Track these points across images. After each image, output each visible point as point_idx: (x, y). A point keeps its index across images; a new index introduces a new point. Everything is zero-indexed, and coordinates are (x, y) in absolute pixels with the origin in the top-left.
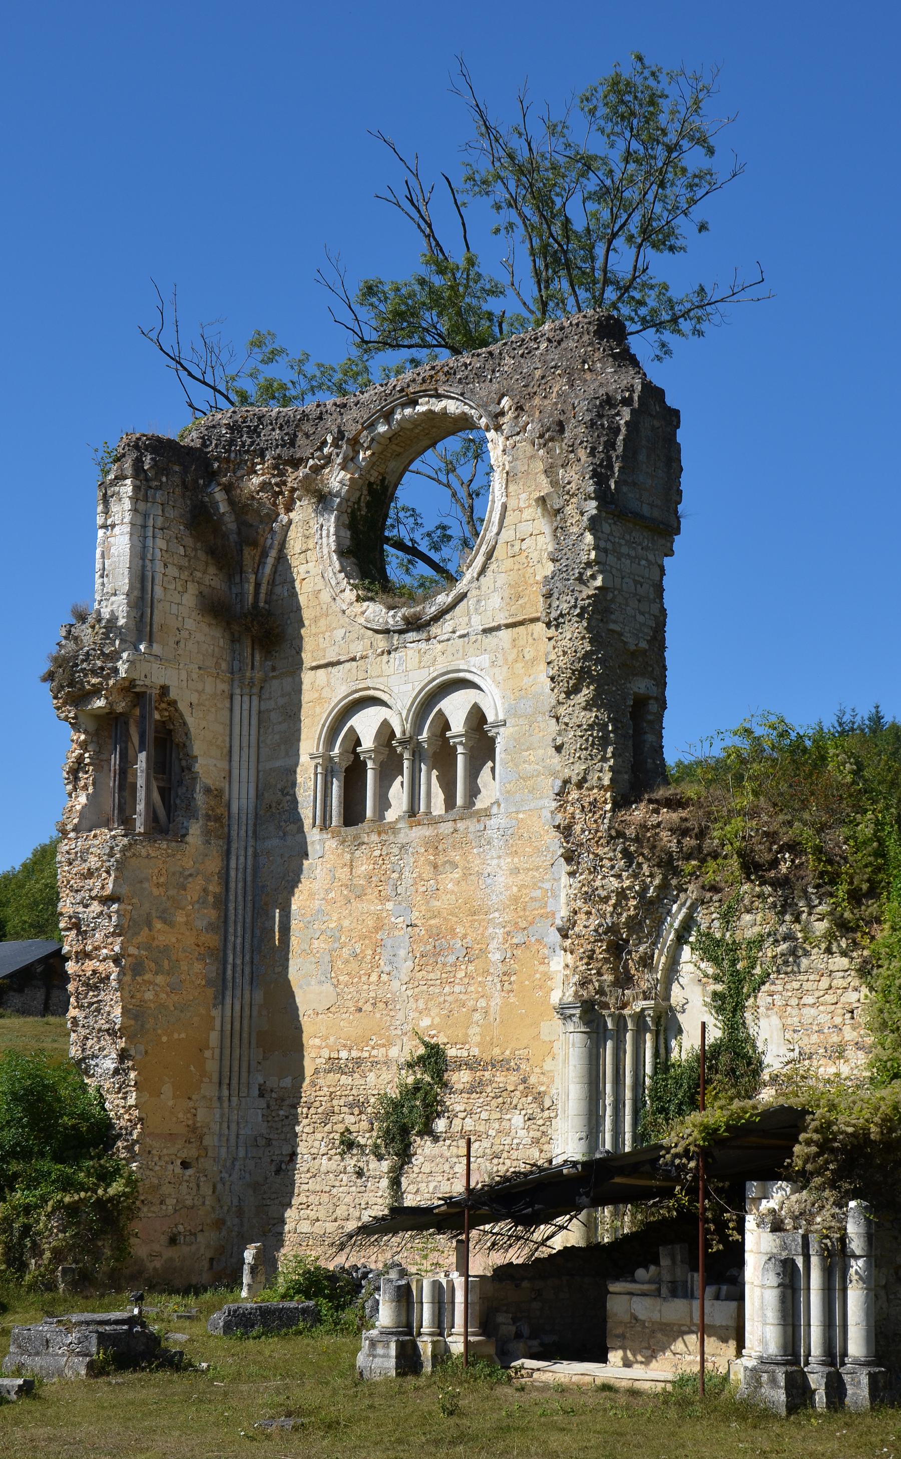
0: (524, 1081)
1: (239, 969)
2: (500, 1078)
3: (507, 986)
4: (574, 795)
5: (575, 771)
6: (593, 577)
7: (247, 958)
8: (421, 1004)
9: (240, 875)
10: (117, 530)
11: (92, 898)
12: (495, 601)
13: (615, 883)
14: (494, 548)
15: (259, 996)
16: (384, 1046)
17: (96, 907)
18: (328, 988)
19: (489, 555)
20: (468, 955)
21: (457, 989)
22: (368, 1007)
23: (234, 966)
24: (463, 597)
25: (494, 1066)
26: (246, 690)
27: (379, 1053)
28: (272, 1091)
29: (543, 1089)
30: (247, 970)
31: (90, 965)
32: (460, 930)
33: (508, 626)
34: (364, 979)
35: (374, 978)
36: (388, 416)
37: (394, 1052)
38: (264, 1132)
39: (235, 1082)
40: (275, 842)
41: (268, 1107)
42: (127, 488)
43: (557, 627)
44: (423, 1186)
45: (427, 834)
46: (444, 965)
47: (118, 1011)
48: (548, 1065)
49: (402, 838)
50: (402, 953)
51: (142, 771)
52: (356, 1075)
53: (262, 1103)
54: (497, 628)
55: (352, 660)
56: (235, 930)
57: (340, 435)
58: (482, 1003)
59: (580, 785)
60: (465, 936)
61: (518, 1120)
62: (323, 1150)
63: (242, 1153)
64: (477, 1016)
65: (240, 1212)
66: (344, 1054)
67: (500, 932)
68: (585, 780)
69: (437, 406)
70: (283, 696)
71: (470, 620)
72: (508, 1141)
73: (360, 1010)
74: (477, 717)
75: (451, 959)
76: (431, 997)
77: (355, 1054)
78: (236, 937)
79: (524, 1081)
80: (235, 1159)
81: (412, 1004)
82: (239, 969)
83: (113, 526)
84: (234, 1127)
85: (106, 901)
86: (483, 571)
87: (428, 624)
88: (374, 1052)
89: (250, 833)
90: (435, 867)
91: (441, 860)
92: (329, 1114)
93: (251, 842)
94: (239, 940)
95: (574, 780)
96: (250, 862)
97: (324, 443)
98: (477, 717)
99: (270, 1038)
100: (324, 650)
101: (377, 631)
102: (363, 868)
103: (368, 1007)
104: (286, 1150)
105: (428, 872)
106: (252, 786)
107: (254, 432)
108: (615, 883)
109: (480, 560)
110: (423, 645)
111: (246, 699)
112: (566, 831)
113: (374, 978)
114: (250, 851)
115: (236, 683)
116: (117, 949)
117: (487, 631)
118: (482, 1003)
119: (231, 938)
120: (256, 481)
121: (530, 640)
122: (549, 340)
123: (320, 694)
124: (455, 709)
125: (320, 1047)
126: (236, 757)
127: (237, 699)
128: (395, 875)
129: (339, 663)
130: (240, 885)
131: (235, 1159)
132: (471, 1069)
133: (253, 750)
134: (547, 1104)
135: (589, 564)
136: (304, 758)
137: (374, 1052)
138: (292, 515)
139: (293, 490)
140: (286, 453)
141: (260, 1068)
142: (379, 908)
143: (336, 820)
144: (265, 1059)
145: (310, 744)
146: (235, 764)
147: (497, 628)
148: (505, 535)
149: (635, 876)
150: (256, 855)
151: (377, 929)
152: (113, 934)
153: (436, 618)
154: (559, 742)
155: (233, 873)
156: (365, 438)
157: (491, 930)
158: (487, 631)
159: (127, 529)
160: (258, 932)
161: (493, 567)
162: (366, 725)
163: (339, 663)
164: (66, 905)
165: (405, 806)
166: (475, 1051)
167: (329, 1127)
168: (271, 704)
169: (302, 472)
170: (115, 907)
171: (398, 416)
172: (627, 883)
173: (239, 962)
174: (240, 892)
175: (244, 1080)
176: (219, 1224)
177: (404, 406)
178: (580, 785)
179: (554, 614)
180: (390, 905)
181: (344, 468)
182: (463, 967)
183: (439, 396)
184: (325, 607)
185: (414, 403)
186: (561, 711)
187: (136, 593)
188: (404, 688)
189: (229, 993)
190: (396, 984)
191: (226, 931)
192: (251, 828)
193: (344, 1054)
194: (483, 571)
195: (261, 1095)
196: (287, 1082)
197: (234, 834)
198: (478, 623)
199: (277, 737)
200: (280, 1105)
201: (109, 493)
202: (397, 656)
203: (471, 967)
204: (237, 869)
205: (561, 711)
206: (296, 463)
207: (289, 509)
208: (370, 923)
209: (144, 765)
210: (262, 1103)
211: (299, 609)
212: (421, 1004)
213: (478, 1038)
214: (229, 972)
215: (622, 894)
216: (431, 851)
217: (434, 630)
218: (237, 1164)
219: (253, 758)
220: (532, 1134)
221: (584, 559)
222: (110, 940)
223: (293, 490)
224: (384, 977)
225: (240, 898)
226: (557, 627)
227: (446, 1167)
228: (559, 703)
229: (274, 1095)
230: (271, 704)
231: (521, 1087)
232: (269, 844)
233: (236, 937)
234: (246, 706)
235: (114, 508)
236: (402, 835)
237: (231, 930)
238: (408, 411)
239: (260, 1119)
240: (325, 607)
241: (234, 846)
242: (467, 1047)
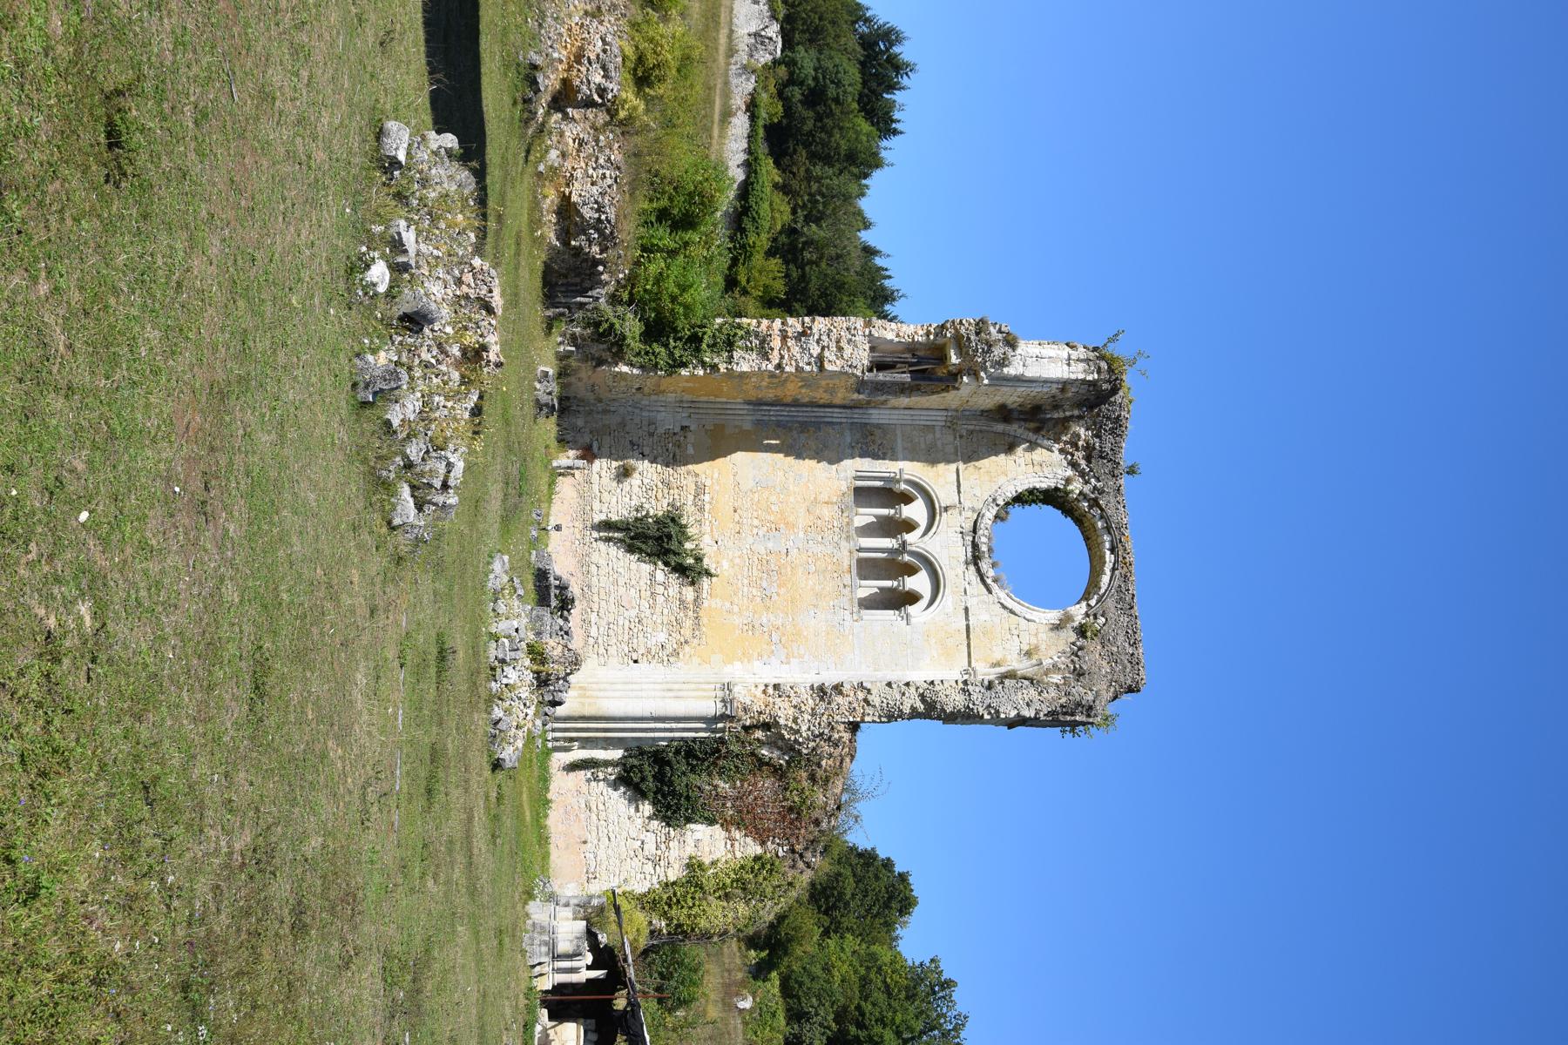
2: (688, 623)
4: (861, 695)
5: (875, 699)
8: (737, 561)
13: (804, 728)
17: (816, 350)
18: (751, 484)
19: (1012, 612)
22: (737, 518)
24: (990, 592)
31: (776, 343)
33: (968, 627)
35: (756, 522)
36: (1108, 529)
40: (848, 439)
48: (696, 660)
49: (844, 544)
53: (677, 430)
54: (967, 619)
57: (1101, 492)
58: (736, 609)
59: (866, 701)
64: (728, 604)
65: (605, 412)
66: (707, 498)
67: (779, 623)
69: (1108, 568)
75: (765, 585)
77: (707, 507)
81: (738, 553)
85: (820, 359)
87: (976, 564)
95: (870, 698)
97: (1098, 480)
99: (717, 444)
103: (737, 518)
104: (647, 451)
107: (1112, 432)
108: (804, 728)
112: (838, 688)
113: (756, 522)
117: (966, 609)
118: (736, 609)
120: (1082, 431)
123: (940, 478)
124: (919, 582)
135: (997, 712)
140: (1095, 453)
151: (787, 524)
153: (978, 570)
156: (1096, 512)
158: (966, 609)
159: (1066, 376)
161: (1005, 613)
162: (915, 511)
164: (821, 324)
166: (706, 604)
168: (938, 435)
171: (1106, 537)
180: (801, 535)
183: (1113, 570)
185: (1112, 550)
186: (913, 689)
190: (750, 540)
196: (691, 450)
200: (673, 451)
205: (913, 689)
206: (1088, 459)
207: (1061, 451)
208: (791, 519)
210: (677, 430)
215: (798, 732)
217: (972, 568)
230: (938, 435)
232: (847, 434)
235: (1081, 366)
238: (1107, 545)
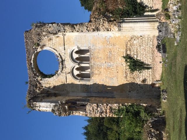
0: (129, 41)
2: (128, 45)
3: (115, 45)
5: (85, 28)
6: (59, 25)
10: (41, 105)
11: (97, 109)
12: (60, 48)
14: (53, 48)
15: (115, 92)
17: (99, 109)
20: (110, 52)
21: (115, 54)
29: (130, 38)
32: (107, 53)
33: (64, 46)
34: (113, 71)
35: (113, 69)
36: (32, 68)
43: (65, 30)
44: (145, 59)
46: (112, 56)
47: (115, 105)
49: (93, 65)
54: (64, 47)
57: (34, 77)
59: (88, 28)
60: (108, 52)
61: (135, 42)
62: (139, 79)
64: (119, 50)
66: (124, 75)
67: (107, 46)
68: (87, 27)
72: (138, 44)
73: (118, 72)
74: (77, 52)
76: (116, 59)
77: (124, 73)
79: (129, 41)
83: (40, 106)
85: (98, 107)
86: (56, 50)
87: (62, 60)
88: (124, 69)
92: (134, 78)
95: (87, 28)
97: (34, 80)
98: (77, 52)
100: (64, 80)
101: (62, 70)
105: (98, 60)
107: (31, 91)
113: (113, 69)
116: (105, 104)
117: (65, 50)
122: (27, 39)
123: (70, 80)
124: (75, 56)
125: (123, 80)
126: (78, 95)
127: (69, 95)
129: (66, 77)
132: (127, 51)
134: (133, 37)
136: (79, 83)
137: (124, 69)
138: (44, 86)
139: (40, 86)
143: (89, 79)
145: (77, 82)
147: (64, 47)
149: (101, 18)
151: (106, 69)
152: (103, 105)
153: (62, 59)
154: (81, 31)
157: (107, 48)
158: (65, 50)
159: (41, 103)
162: (76, 73)
163: (66, 77)
164: (97, 115)
166: (125, 50)
167: (135, 78)
169: (38, 84)
170: (99, 104)
172: (102, 19)
177: (31, 66)
178: (88, 28)
179: (63, 31)
180: (102, 67)
181: (38, 77)
183: (31, 59)
185: (31, 64)
188: (71, 65)
193: (124, 75)
194: (56, 50)
195: (130, 92)
196: (128, 86)
198: (63, 51)
201: (35, 106)
203: (112, 51)
206: (37, 85)
207: (43, 87)
212: (117, 60)
213: (123, 50)
217: (63, 59)
220: (137, 39)
222: (104, 106)
223: (40, 86)
226: (65, 30)
227: (142, 55)
228: (76, 30)
230: (71, 90)
231: (130, 41)
236: (92, 64)
238: (32, 65)
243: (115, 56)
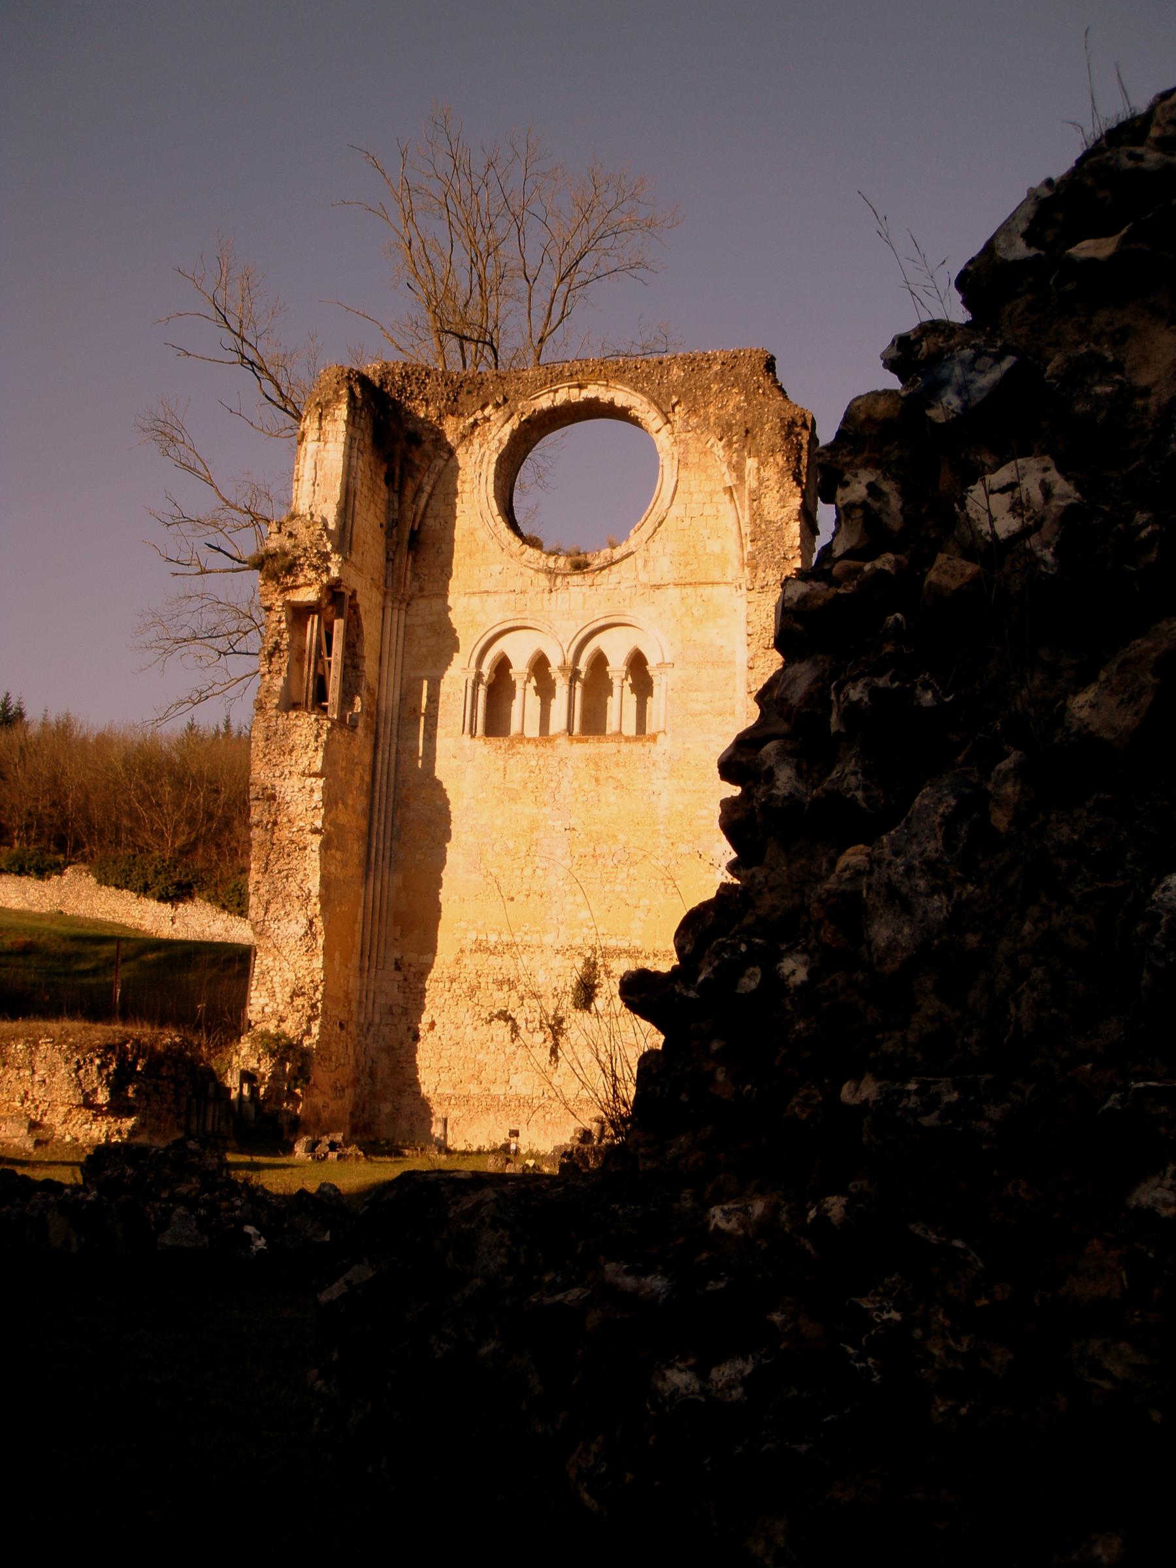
1: (381, 853)
7: (388, 844)
9: (385, 769)
16: (538, 932)
23: (377, 849)
25: (655, 955)
26: (396, 605)
27: (533, 939)
28: (410, 965)
30: (387, 854)
34: (517, 872)
35: (528, 871)
37: (549, 939)
38: (401, 1002)
39: (374, 955)
41: (405, 979)
42: (342, 411)
45: (588, 751)
50: (559, 852)
51: (336, 663)
52: (507, 956)
53: (399, 976)
55: (493, 590)
56: (379, 818)
63: (377, 1019)
70: (431, 614)
71: (637, 576)
73: (512, 899)
78: (379, 823)
80: (370, 1025)
82: (381, 853)
84: (371, 996)
88: (527, 938)
89: (395, 732)
90: (597, 780)
91: (603, 775)
93: (395, 740)
94: (382, 828)
96: (393, 757)
102: (517, 775)
106: (398, 689)
109: (648, 528)
110: (585, 589)
111: (396, 612)
113: (528, 871)
114: (394, 750)
115: (389, 597)
119: (376, 824)
121: (699, 600)
128: (553, 784)
130: (385, 777)
131: (370, 1025)
133: (399, 659)
141: (396, 944)
142: (535, 811)
144: (402, 935)
146: (385, 667)
148: (674, 511)
150: (398, 752)
151: (532, 830)
155: (379, 766)
160: (397, 823)
165: (564, 726)
173: (381, 847)
174: (384, 783)
175: (382, 954)
176: (357, 1081)
180: (547, 810)
182: (625, 869)
184: (481, 544)
187: (342, 504)
189: (372, 874)
191: (371, 818)
192: (395, 727)
193: (493, 938)
197: (381, 730)
199: (424, 650)
202: (560, 596)
204: (383, 763)
209: (339, 658)
210: (399, 976)
211: (452, 540)
214: (373, 855)
216: (591, 765)
218: (373, 1029)
219: (399, 667)
221: (789, 543)
224: (539, 872)
225: (384, 789)
229: (412, 969)
233: (379, 823)
234: (395, 619)
237: (376, 817)
239: (396, 990)
240: (481, 544)
241: (381, 741)
242: (628, 938)
243: (608, 887)
